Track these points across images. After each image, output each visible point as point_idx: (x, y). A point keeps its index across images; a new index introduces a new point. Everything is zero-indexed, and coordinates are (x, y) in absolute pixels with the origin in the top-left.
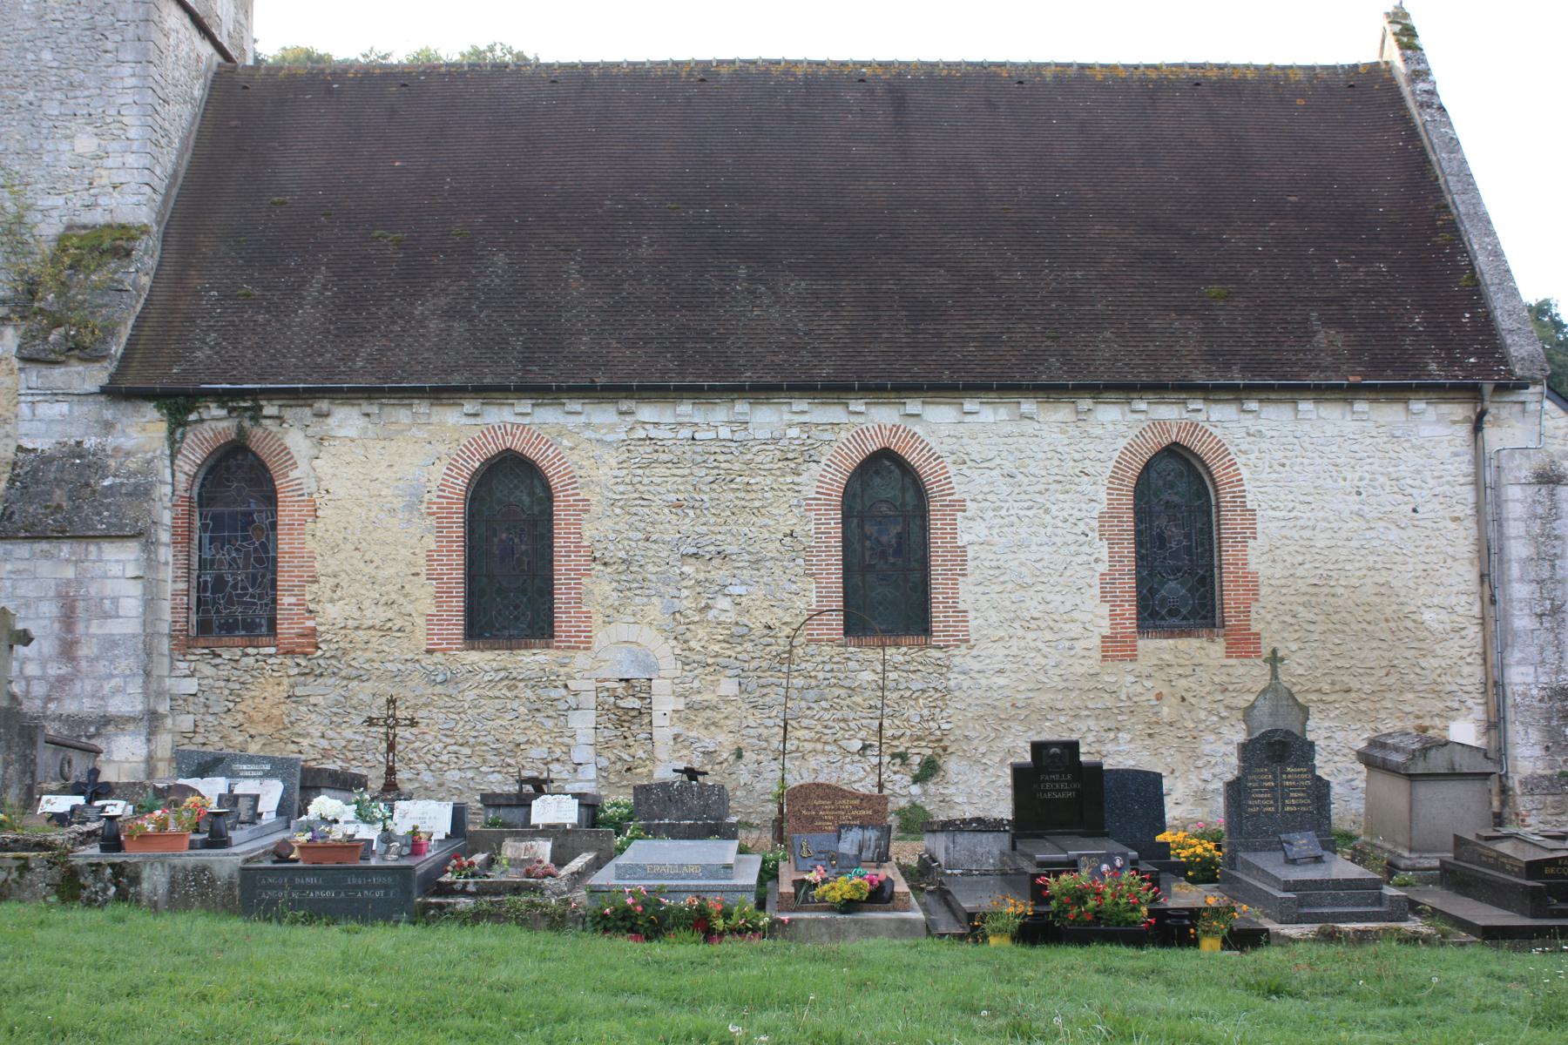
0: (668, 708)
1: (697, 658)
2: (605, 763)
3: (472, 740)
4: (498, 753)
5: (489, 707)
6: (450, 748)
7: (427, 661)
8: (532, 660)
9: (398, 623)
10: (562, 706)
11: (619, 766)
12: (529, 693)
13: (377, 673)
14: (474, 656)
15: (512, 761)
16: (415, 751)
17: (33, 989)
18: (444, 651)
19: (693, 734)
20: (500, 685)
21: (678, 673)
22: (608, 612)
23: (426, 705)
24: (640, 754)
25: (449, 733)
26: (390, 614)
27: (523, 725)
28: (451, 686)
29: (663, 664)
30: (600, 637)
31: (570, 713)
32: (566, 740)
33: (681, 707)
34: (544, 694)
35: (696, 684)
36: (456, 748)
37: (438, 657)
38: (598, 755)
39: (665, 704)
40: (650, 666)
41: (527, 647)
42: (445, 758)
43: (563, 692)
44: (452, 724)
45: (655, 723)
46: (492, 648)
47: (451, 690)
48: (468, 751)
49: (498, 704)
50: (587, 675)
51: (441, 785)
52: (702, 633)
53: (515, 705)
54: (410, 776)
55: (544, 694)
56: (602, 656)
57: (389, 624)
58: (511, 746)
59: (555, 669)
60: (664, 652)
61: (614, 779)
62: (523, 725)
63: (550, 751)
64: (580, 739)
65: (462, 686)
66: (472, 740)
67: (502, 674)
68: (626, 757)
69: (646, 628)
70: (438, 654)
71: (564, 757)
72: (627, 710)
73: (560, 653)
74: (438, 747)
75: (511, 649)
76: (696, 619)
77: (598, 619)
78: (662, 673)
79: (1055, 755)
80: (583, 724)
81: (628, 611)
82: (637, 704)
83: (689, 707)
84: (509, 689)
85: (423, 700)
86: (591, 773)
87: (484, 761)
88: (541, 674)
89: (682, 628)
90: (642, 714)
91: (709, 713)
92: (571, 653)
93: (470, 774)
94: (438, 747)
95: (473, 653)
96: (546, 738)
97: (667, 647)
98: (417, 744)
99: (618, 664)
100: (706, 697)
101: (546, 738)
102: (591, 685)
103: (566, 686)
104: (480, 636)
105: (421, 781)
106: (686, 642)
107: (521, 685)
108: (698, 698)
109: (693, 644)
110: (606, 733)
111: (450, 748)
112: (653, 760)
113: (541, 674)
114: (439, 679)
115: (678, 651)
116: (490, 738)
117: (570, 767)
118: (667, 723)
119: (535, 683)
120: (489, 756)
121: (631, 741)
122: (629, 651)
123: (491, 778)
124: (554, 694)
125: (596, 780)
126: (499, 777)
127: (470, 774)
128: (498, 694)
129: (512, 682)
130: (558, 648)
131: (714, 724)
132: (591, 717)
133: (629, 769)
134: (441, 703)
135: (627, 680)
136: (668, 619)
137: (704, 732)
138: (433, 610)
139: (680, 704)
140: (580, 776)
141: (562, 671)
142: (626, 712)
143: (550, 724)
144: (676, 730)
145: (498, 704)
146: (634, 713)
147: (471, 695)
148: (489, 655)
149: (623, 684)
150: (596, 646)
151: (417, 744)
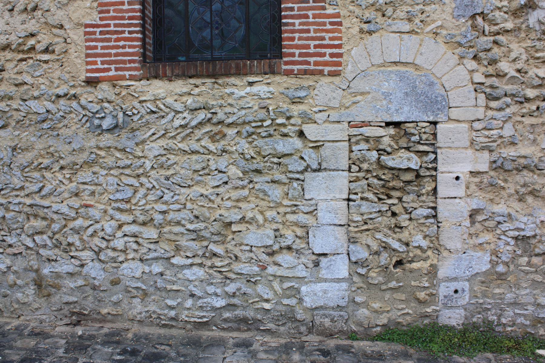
0: (463, 169)
1: (510, 88)
2: (363, 254)
3: (158, 218)
4: (197, 236)
5: (183, 167)
6: (126, 229)
7: (88, 96)
8: (248, 93)
9: (44, 39)
10: (295, 165)
11: (384, 259)
12: (244, 145)
13: (17, 116)
14: (158, 88)
15: (219, 249)
16: (76, 231)
17: (157, 118)
18: (113, 81)
19: (501, 208)
20: (199, 133)
21: (480, 113)
22: (369, 14)
23: (88, 164)
24: (419, 240)
25: (125, 205)
26: (32, 26)
27: (235, 194)
28: (124, 134)
29: (454, 98)
30: (357, 55)
31: (308, 175)
32: (302, 218)
33: (484, 167)
34: (266, 146)
35: (508, 131)
36: (134, 228)
37: (105, 90)
38: (352, 240)
39: (458, 163)
40: (437, 102)
41: (239, 73)
42: (119, 243)
43: (298, 143)
44: (129, 193)
45: (441, 192)
46: (186, 75)
47: (124, 141)
48: (151, 233)
49: (196, 162)
50: (334, 116)
51: (115, 283)
52: (517, 49)
53: (222, 163)
54: (70, 268)
55: (266, 146)
56: (359, 85)
57: (32, 42)
58: (217, 227)
59: (285, 106)
60: (456, 76)
61: (375, 277)
62: (235, 194)
63: (278, 235)
64: (324, 216)
65: (141, 135)
66: (158, 218)
67: (202, 115)
68: (396, 245)
69: (429, 41)
70: (104, 86)
71: (299, 244)
72: (397, 172)
73: (292, 81)
74: (109, 226)
75: (214, 75)
76: (509, 25)
77: (351, 27)
78: (454, 114)
79: (183, 56)
80: (329, 192)
81: (401, 13)
82: (414, 162)
83: (497, 166)
84: (213, 138)
85: (84, 156)
86: (341, 268)
87: (178, 249)
88: (262, 114)
89: (485, 41)
90: (422, 178)
91: (527, 176)
92: (307, 81)
93: (157, 268)
94: (109, 226)
95: (157, 83)
96: (270, 214)
97: (462, 73)
98: (79, 222)
99: (382, 100)
100: (524, 151)
101: (270, 214)
102: (340, 132)
103: (301, 134)
104: (172, 59)
105: (86, 278)
106: (493, 62)
107: (231, 132)
108: (511, 152)
109: (504, 66)
110: (365, 207)
111: (126, 229)
112: (437, 248)
113: (262, 114)
114: (106, 124)
115: (479, 78)
116: (185, 214)
117: (307, 259)
118: (461, 192)
119: (252, 130)
120: (183, 242)
121: (403, 219)
122: (402, 78)
123: (188, 273)
124: (282, 146)
125: (349, 280)
126: (200, 273)
127: (157, 268)
128: (196, 146)
129: (217, 127)
130: (288, 73)
131: (533, 193)
132: (341, 182)
133: (399, 263)
134: (110, 161)
135: (397, 125)
136: (464, 24)
137: (517, 205)
138: (94, 18)
139: (483, 162)
140: (324, 273)
141: (296, 110)
142: (396, 172)
143: (276, 192)
144: (474, 204)
145: (196, 162)
146: (409, 177)
147: (155, 148)
148: (180, 86)
149: (392, 131)
150: (349, 71)
151: (79, 222)
